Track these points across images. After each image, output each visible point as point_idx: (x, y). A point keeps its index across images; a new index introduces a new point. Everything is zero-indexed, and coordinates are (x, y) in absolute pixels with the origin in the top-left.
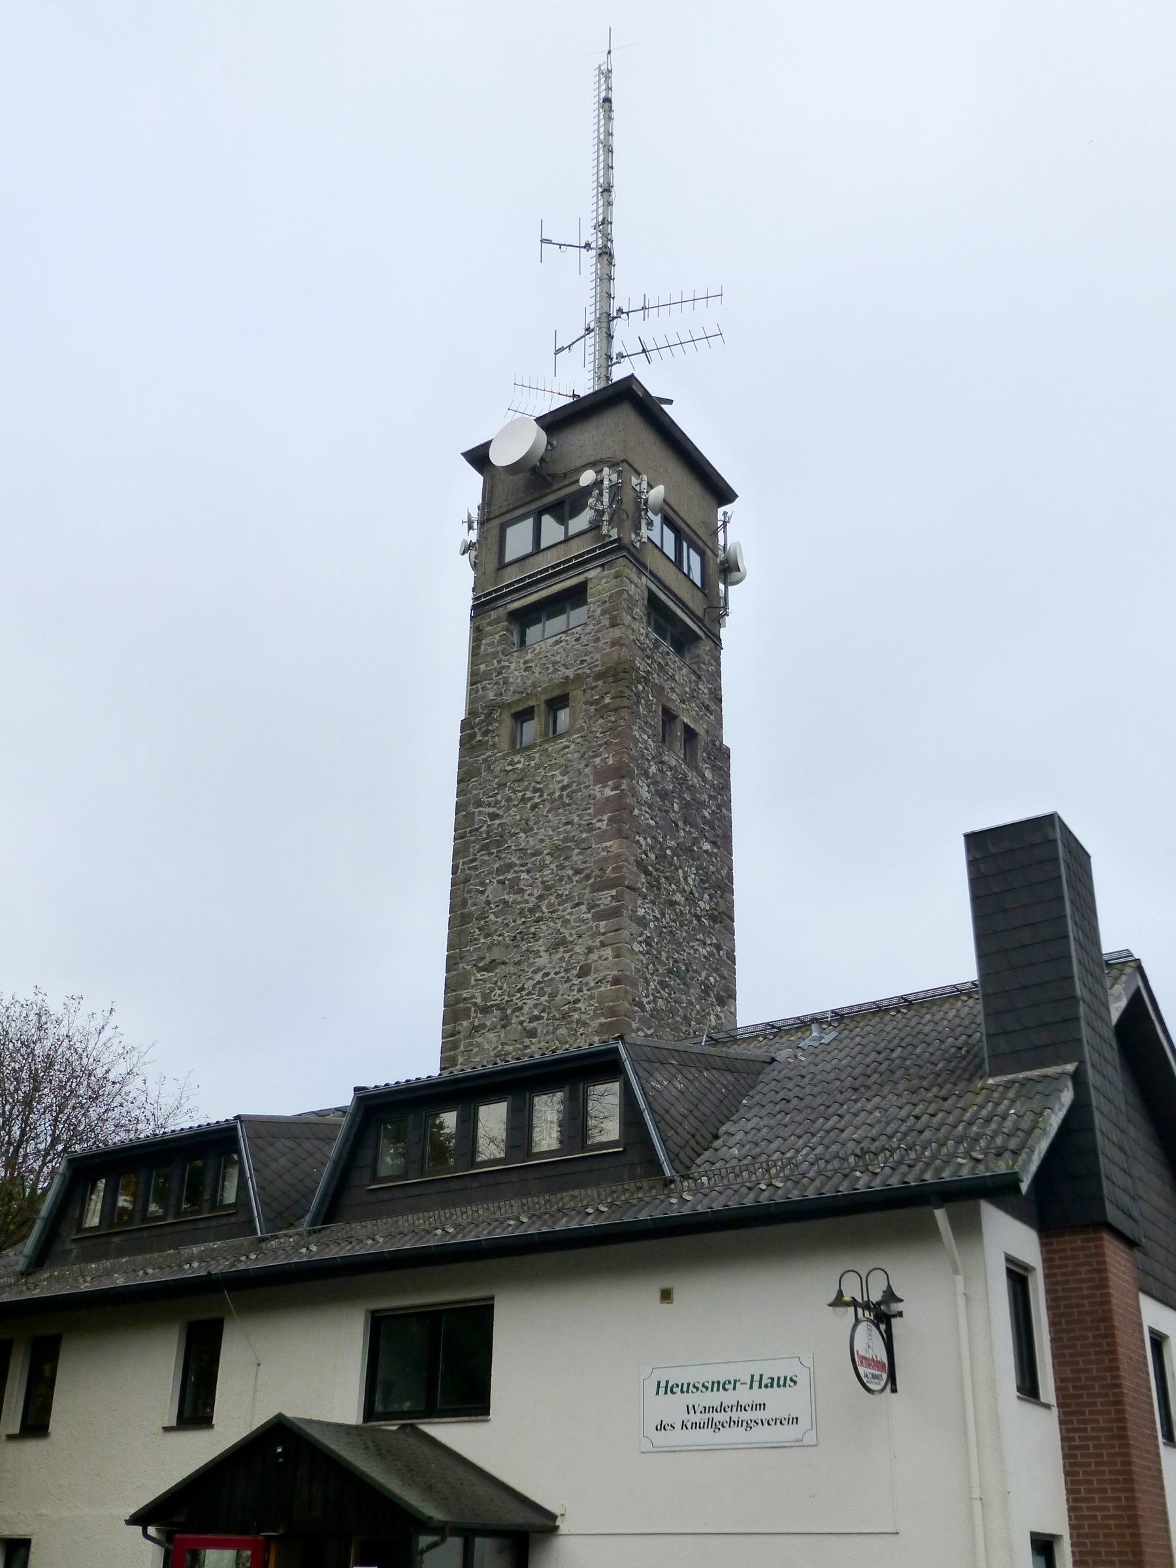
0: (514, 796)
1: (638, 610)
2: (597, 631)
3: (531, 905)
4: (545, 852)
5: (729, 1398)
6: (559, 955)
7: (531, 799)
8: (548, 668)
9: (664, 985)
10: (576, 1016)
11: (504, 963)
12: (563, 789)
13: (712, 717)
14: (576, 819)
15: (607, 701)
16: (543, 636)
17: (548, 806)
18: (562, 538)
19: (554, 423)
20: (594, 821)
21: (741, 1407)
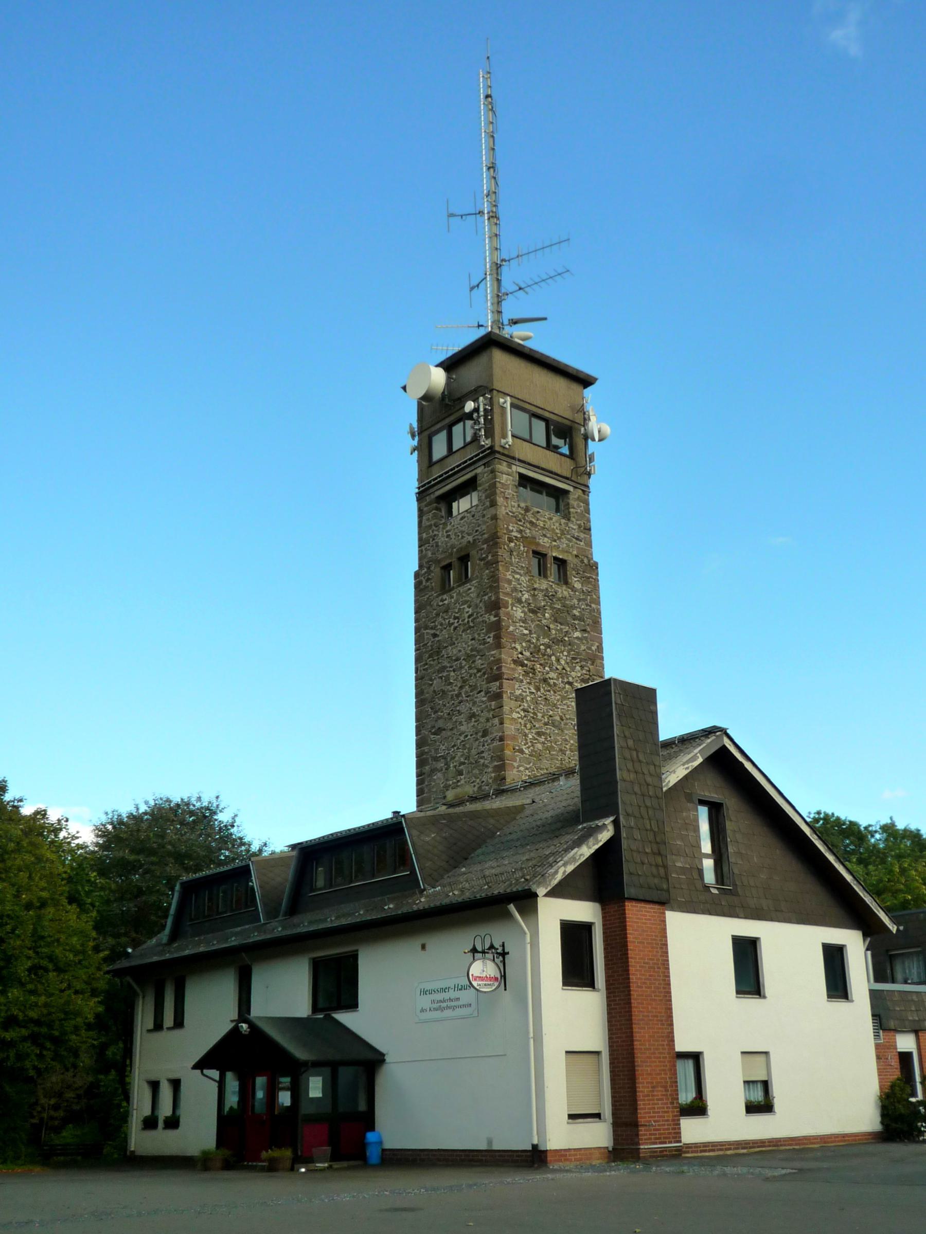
0: (444, 622)
1: (510, 491)
2: (484, 510)
3: (456, 692)
4: (462, 658)
5: (446, 996)
6: (472, 724)
7: (453, 624)
8: (459, 536)
9: (539, 734)
10: (482, 761)
11: (444, 730)
12: (469, 617)
13: (582, 543)
14: (477, 636)
15: (490, 558)
16: (459, 511)
17: (462, 628)
18: (462, 445)
19: (451, 365)
20: (486, 638)
21: (451, 1000)
